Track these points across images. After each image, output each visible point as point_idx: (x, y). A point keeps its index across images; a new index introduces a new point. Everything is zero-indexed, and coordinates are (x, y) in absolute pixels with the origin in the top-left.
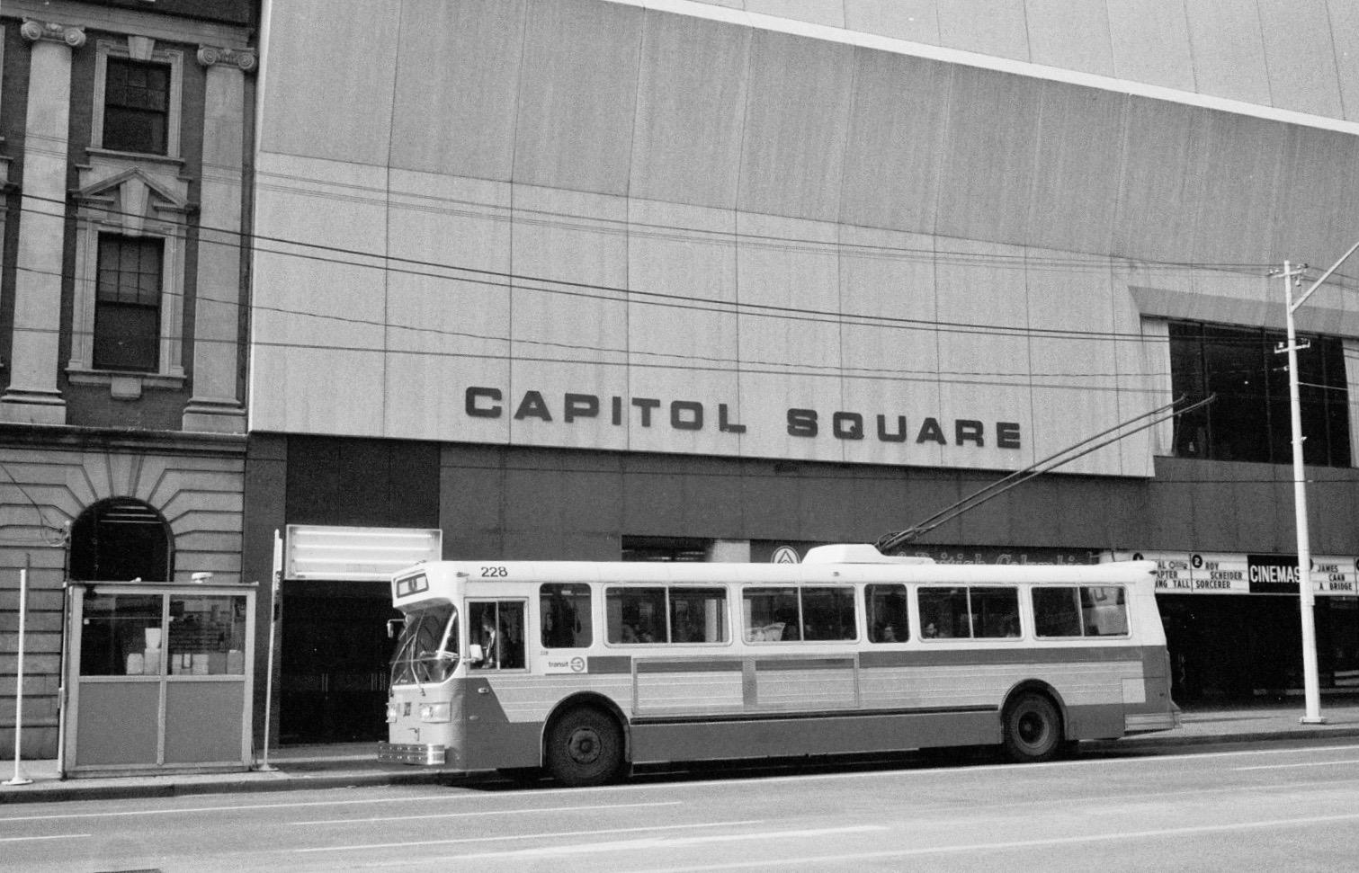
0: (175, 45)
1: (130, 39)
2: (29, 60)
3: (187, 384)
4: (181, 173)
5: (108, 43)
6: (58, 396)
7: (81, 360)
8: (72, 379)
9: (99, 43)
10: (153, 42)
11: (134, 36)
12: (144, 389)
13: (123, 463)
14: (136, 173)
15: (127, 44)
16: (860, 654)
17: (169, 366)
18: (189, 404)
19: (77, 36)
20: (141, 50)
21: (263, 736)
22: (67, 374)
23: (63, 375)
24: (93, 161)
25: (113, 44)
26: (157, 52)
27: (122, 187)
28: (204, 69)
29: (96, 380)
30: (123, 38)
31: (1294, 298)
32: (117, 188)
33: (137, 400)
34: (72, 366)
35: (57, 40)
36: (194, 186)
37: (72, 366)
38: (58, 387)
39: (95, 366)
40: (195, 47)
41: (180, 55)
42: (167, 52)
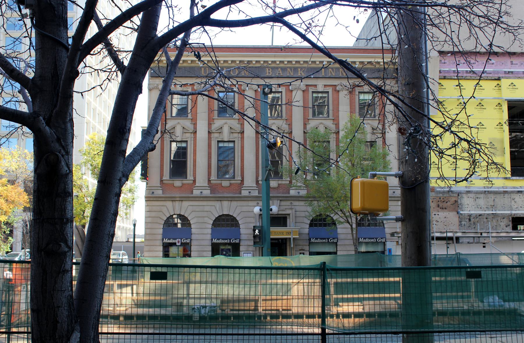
2: (339, 95)
3: (194, 181)
4: (333, 122)
7: (214, 177)
8: (164, 182)
9: (310, 88)
13: (225, 203)
16: (286, 255)
17: (190, 177)
18: (195, 187)
19: (304, 88)
20: (320, 88)
22: (162, 181)
23: (162, 181)
24: (310, 121)
25: (313, 88)
26: (325, 89)
29: (171, 182)
30: (315, 86)
31: (90, 118)
33: (181, 187)
34: (164, 178)
35: (298, 89)
36: (195, 125)
37: (164, 178)
38: (160, 185)
39: (218, 178)
42: (328, 88)
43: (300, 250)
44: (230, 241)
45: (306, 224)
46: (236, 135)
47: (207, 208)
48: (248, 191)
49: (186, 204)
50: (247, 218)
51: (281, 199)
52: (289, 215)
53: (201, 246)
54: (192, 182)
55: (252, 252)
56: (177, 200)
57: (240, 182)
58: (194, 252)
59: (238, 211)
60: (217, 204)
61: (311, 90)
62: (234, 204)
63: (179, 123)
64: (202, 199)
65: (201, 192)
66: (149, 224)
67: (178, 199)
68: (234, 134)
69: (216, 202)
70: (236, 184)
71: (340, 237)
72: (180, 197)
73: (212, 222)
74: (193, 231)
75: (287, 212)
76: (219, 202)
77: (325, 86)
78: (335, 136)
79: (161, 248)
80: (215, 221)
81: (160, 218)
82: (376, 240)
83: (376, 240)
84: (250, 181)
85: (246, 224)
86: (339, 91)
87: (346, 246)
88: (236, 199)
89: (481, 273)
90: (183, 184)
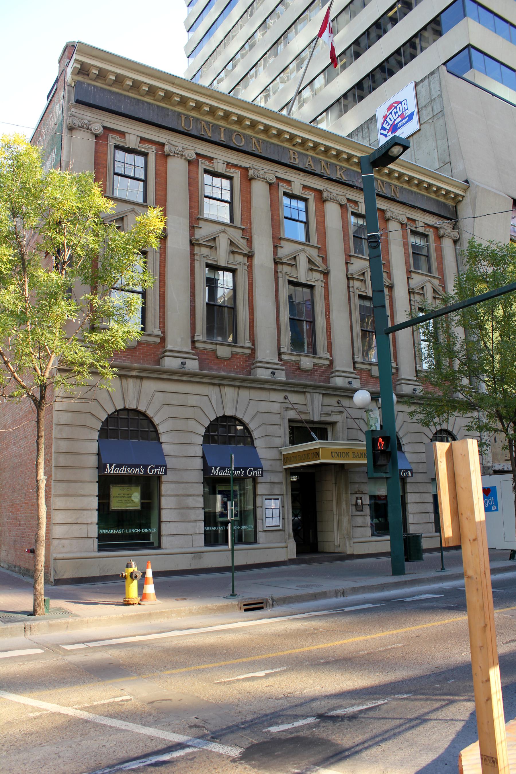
0: (236, 166)
1: (215, 160)
2: (166, 164)
5: (115, 136)
6: (193, 354)
7: (201, 335)
9: (110, 136)
10: (139, 139)
11: (129, 133)
12: (315, 365)
13: (229, 392)
14: (133, 210)
15: (213, 163)
18: (332, 373)
19: (98, 128)
21: (132, 540)
25: (117, 137)
26: (141, 145)
27: (125, 219)
28: (167, 156)
30: (122, 134)
32: (214, 239)
40: (163, 145)
41: (154, 148)
43: (356, 493)
44: (146, 471)
45: (197, 436)
46: (240, 258)
47: (193, 400)
48: (180, 361)
49: (150, 386)
50: (268, 426)
51: (324, 392)
52: (333, 424)
53: (183, 485)
54: (158, 340)
55: (280, 497)
56: (132, 377)
57: (158, 340)
58: (168, 498)
59: (251, 411)
60: (213, 392)
61: (204, 165)
62: (245, 394)
63: (224, 232)
64: (184, 378)
65: (183, 364)
66: (67, 428)
67: (134, 374)
68: (314, 273)
69: (211, 388)
70: (242, 354)
71: (170, 462)
72: (140, 370)
73: (203, 431)
74: (166, 448)
75: (334, 418)
76: (216, 389)
77: (305, 187)
78: (246, 262)
79: (94, 489)
80: (208, 429)
81: (93, 415)
82: (245, 473)
83: (245, 473)
84: (268, 352)
85: (268, 438)
86: (168, 155)
87: (418, 484)
88: (249, 385)
89: (205, 543)
90: (233, 354)
